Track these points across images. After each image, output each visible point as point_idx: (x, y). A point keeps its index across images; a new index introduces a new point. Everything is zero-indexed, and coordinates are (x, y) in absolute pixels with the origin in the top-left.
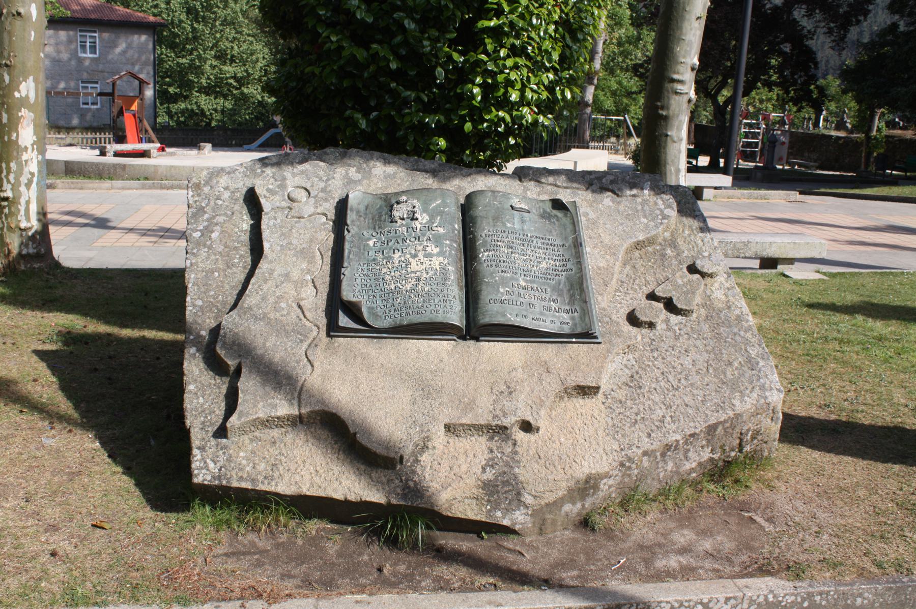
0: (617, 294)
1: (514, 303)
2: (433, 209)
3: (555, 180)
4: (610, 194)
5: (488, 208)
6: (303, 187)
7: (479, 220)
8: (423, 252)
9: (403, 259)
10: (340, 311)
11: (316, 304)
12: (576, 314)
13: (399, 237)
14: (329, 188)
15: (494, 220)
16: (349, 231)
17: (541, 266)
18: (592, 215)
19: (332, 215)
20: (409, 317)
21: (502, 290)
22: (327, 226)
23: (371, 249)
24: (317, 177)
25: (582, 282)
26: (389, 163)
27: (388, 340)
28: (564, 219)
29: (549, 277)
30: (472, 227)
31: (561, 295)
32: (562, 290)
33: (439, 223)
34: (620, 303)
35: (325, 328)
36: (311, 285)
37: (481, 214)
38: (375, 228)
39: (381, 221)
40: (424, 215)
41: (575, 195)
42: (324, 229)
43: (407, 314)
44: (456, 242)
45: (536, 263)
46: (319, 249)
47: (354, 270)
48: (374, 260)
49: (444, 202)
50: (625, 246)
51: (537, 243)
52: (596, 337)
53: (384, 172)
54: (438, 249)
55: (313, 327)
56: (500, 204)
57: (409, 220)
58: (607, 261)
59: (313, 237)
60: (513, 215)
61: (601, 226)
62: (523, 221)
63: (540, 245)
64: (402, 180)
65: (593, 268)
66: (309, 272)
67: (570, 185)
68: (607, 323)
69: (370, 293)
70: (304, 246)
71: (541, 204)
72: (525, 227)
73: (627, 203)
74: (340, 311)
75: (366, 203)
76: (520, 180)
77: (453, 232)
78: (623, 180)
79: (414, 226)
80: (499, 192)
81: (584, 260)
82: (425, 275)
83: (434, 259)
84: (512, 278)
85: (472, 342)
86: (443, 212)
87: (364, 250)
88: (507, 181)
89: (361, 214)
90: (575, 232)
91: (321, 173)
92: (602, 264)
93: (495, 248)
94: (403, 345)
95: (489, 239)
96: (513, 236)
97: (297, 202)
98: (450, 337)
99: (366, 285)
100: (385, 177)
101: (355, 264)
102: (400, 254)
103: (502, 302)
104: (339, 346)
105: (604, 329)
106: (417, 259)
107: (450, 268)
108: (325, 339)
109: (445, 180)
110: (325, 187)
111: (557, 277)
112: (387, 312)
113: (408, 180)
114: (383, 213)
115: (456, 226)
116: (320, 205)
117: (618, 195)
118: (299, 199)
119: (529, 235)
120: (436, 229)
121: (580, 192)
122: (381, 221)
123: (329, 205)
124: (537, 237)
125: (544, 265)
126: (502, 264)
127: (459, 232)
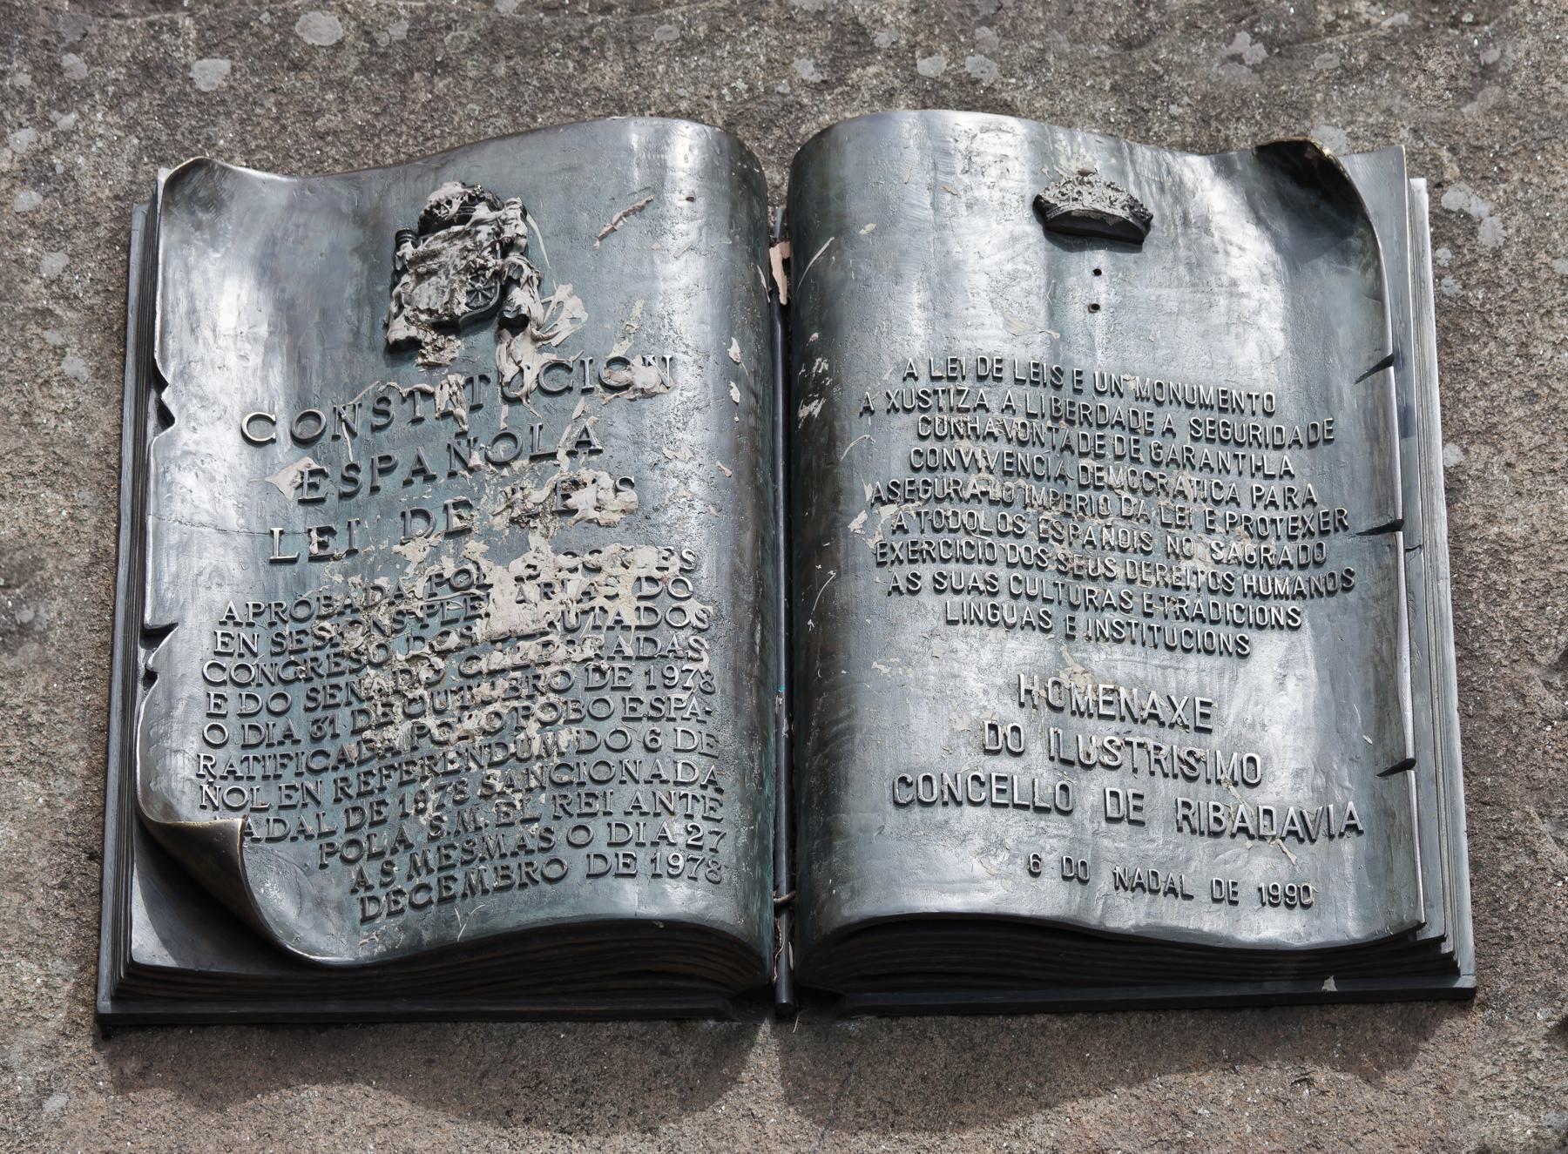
9: (449, 569)
106: (518, 567)
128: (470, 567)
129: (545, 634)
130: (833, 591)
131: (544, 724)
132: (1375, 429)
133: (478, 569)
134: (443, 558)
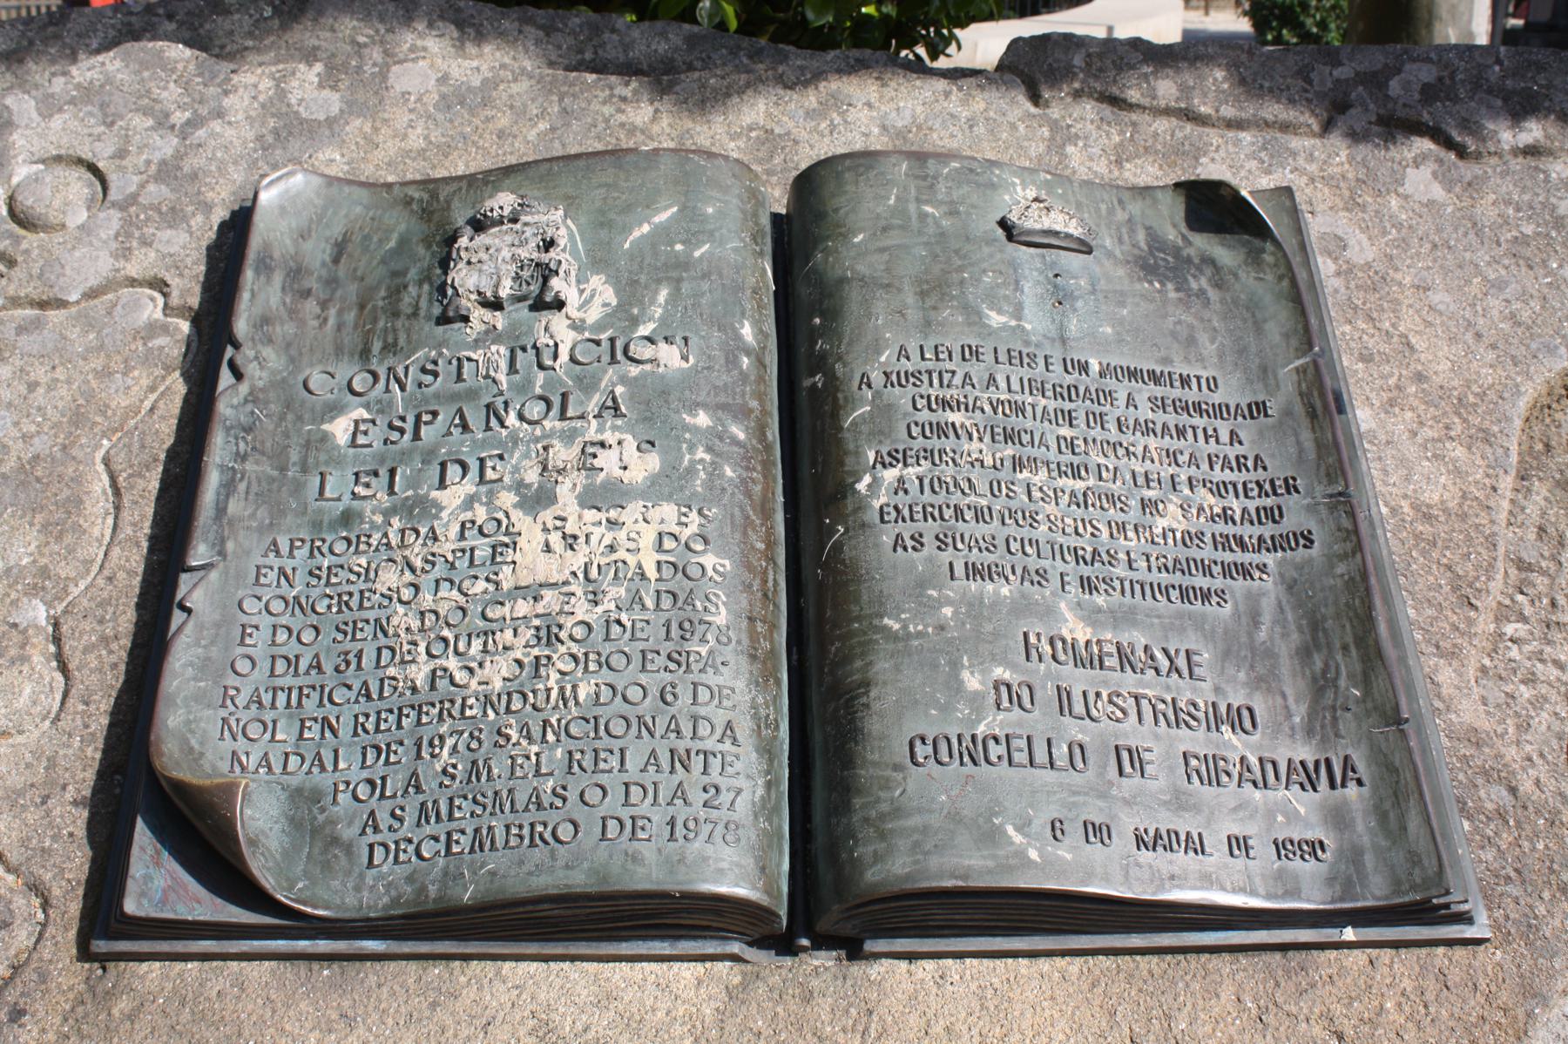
0: (1509, 629)
1: (1041, 755)
2: (636, 254)
3: (1185, 90)
4: (1424, 145)
5: (893, 239)
6: (80, 161)
7: (854, 295)
8: (581, 479)
9: (481, 514)
10: (140, 825)
11: (52, 764)
12: (1352, 790)
13: (472, 394)
14: (191, 163)
15: (923, 295)
16: (238, 375)
17: (1161, 524)
18: (1362, 249)
19: (188, 288)
20: (493, 862)
21: (972, 682)
22: (161, 341)
23: (338, 461)
24: (146, 112)
25: (1370, 607)
26: (480, 38)
27: (393, 966)
28: (1247, 278)
29: (1201, 581)
30: (822, 332)
31: (1264, 682)
32: (1270, 654)
33: (664, 322)
34: (1530, 680)
35: (75, 908)
36: (40, 656)
37: (862, 268)
38: (365, 354)
39: (396, 314)
40: (596, 281)
41: (1280, 156)
42: (147, 359)
43: (477, 844)
44: (742, 413)
45: (1134, 514)
46: (107, 462)
47: (240, 576)
48: (347, 518)
49: (688, 212)
50: (1530, 391)
51: (1130, 401)
52: (1465, 918)
53: (444, 79)
54: (653, 461)
55: (19, 902)
56: (953, 213)
57: (522, 312)
58: (1457, 472)
59: (90, 396)
60: (1014, 265)
61: (1408, 297)
62: (1061, 299)
63: (1145, 412)
64: (520, 113)
65: (1394, 511)
66: (41, 581)
67: (1249, 110)
68: (1501, 815)
69: (310, 705)
70: (40, 445)
71: (1136, 207)
72: (1073, 326)
73: (1507, 187)
74: (140, 825)
75: (337, 231)
76: (1035, 98)
77: (731, 361)
78: (1478, 84)
79: (544, 340)
80: (945, 157)
81: (1359, 481)
82: (582, 610)
83: (631, 513)
84: (1022, 607)
85: (824, 960)
86: (683, 264)
87: (305, 469)
88: (982, 102)
89: (312, 283)
90: (1310, 346)
91: (170, 94)
92: (1438, 490)
93: (935, 443)
94: (469, 994)
95: (901, 397)
96: (1017, 373)
97: (48, 228)
98: (711, 947)
99: (292, 663)
100: (445, 103)
101: (248, 548)
102: (469, 487)
103: (975, 751)
104: (131, 1017)
105: (1489, 855)
106: (547, 516)
107: (709, 560)
108: (68, 973)
109: (704, 102)
110: (179, 156)
111: (1240, 584)
112: (384, 819)
113: (542, 115)
114: (413, 274)
115: (747, 332)
116: (146, 243)
117: (1462, 152)
118: (54, 217)
119: (1095, 367)
120: (646, 352)
121: (1295, 143)
122: (396, 314)
123: (183, 237)
124: (1133, 374)
125: (1171, 518)
126: (970, 527)
127: (760, 363)
128: (500, 515)
129: (566, 583)
130: (842, 545)
131: (562, 673)
132: (1312, 407)
133: (508, 517)
134: (476, 505)
